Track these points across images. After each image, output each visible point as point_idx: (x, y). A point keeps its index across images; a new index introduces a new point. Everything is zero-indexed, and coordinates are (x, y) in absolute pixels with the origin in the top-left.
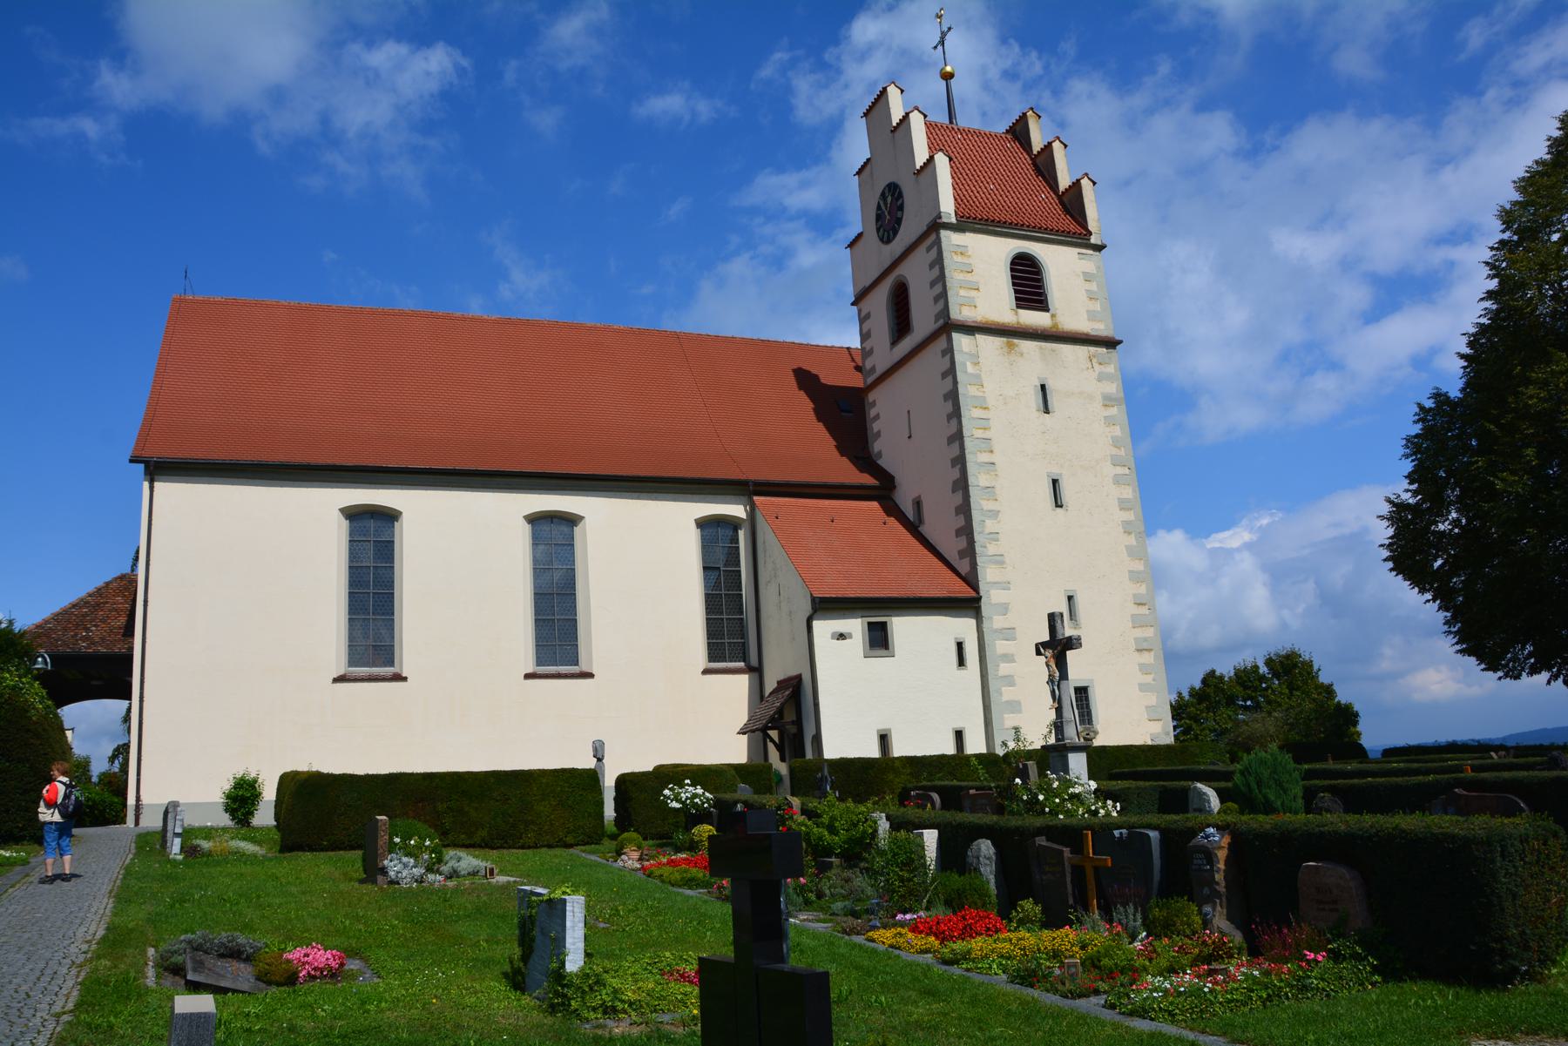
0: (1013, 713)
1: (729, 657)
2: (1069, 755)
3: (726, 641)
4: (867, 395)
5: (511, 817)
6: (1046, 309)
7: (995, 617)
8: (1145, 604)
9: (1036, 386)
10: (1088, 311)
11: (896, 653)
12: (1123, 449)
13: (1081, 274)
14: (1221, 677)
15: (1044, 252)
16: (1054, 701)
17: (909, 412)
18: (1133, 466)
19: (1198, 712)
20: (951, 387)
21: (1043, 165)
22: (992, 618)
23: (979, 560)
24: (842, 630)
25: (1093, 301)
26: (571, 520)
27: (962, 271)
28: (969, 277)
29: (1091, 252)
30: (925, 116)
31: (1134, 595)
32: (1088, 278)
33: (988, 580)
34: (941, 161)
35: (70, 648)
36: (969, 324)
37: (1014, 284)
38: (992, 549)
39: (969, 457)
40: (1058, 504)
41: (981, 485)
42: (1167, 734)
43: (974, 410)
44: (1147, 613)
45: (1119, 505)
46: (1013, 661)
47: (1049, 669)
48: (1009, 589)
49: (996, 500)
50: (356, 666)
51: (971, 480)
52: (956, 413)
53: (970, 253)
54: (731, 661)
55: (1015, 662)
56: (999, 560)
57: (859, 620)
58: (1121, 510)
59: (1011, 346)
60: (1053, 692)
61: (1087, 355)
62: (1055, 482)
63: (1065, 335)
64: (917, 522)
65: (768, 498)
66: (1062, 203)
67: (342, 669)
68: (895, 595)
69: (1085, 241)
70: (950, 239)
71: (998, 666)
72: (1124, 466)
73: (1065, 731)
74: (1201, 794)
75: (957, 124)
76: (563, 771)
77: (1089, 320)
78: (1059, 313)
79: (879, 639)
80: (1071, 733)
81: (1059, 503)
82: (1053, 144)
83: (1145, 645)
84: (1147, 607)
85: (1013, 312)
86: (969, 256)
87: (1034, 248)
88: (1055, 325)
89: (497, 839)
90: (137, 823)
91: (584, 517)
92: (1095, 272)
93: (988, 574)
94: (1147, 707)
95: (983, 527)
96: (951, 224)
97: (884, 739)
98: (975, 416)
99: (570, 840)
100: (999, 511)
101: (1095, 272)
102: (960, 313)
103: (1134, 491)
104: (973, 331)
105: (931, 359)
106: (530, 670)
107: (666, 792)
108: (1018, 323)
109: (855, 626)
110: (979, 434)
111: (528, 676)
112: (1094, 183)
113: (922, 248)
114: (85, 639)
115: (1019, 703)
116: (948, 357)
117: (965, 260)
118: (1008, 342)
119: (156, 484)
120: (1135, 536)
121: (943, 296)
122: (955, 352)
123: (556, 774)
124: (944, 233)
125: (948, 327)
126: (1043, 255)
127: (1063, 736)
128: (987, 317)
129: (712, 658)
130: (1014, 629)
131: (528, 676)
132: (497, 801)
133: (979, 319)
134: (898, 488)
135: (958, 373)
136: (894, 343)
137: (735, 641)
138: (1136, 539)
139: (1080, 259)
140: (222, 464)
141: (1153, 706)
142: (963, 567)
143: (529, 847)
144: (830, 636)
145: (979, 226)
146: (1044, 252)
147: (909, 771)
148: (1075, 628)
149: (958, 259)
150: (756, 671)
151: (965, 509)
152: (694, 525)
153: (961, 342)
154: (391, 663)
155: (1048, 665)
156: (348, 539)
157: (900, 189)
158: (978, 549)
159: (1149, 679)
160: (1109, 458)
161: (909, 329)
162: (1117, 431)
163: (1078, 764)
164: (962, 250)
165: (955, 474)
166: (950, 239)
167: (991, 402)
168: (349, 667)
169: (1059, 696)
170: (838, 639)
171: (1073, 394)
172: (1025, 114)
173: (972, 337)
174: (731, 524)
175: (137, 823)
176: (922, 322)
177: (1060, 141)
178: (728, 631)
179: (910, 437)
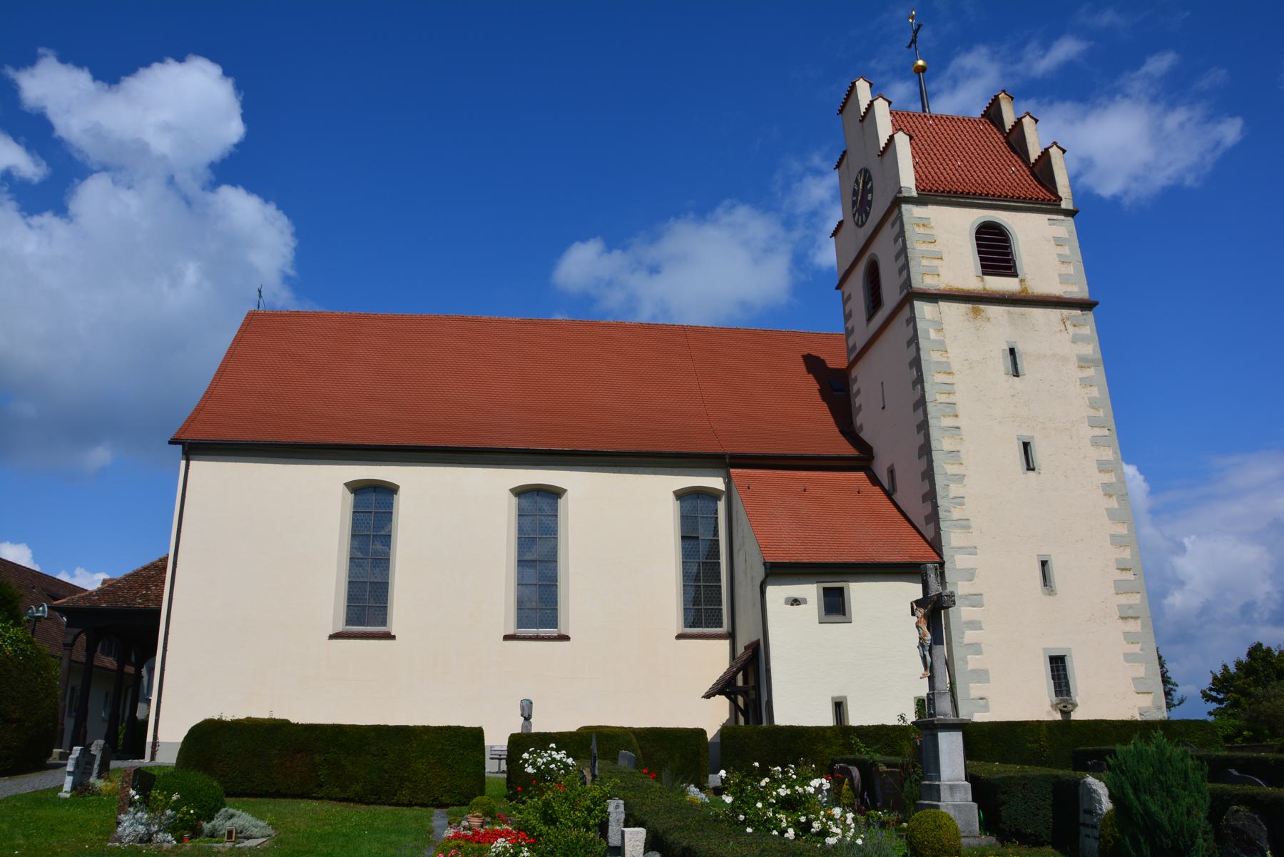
0: (979, 682)
1: (705, 623)
2: (939, 734)
3: (703, 607)
4: (850, 372)
5: (386, 773)
6: (1015, 275)
7: (959, 583)
8: (1130, 570)
9: (1004, 350)
10: (1060, 275)
11: (853, 618)
12: (1101, 410)
13: (1052, 239)
14: (1269, 650)
15: (1014, 222)
16: (926, 670)
17: (882, 383)
18: (1113, 427)
19: (1246, 686)
20: (914, 354)
21: (1016, 140)
22: (957, 583)
23: (942, 525)
24: (797, 595)
25: (1066, 265)
26: (554, 494)
27: (924, 242)
28: (931, 247)
29: (1062, 217)
30: (890, 103)
31: (1117, 560)
32: (1059, 242)
33: (952, 545)
34: (902, 141)
35: (127, 604)
36: (931, 292)
37: (979, 252)
38: (956, 514)
39: (931, 422)
40: (1030, 467)
41: (944, 449)
42: (1159, 708)
43: (938, 375)
44: (1133, 579)
45: (1098, 468)
46: (981, 628)
47: (919, 631)
48: (976, 554)
49: (962, 464)
50: (353, 625)
51: (934, 445)
52: (919, 380)
53: (932, 224)
54: (708, 627)
55: (982, 629)
56: (965, 525)
57: (815, 585)
58: (1100, 471)
59: (977, 312)
60: (924, 658)
61: (1059, 317)
62: (1026, 446)
63: (1035, 298)
64: (891, 490)
65: (745, 470)
66: (1033, 174)
67: (340, 627)
68: (852, 560)
69: (1055, 207)
70: (911, 213)
71: (964, 633)
72: (1103, 427)
73: (937, 705)
74: (1091, 792)
75: (930, 112)
76: (449, 728)
77: (1061, 283)
78: (1028, 277)
79: (835, 605)
80: (944, 705)
81: (1031, 466)
82: (1023, 120)
83: (1130, 613)
84: (1132, 572)
85: (979, 279)
86: (932, 227)
87: (1000, 217)
88: (1025, 290)
89: (371, 795)
90: (153, 758)
91: (566, 490)
92: (1067, 236)
93: (952, 539)
94: (1134, 679)
95: (947, 491)
96: (912, 197)
97: (839, 707)
98: (939, 381)
99: (445, 799)
100: (964, 475)
101: (1067, 236)
102: (923, 282)
103: (1115, 453)
104: (937, 299)
105: (898, 330)
106: (511, 631)
107: (526, 755)
108: (984, 289)
109: (811, 592)
110: (942, 398)
111: (507, 638)
112: (1064, 151)
113: (888, 226)
114: (143, 596)
115: (986, 672)
116: (911, 325)
117: (928, 231)
118: (973, 308)
119: (192, 463)
120: (1117, 498)
121: (906, 267)
122: (917, 320)
123: (439, 731)
124: (905, 207)
125: (912, 296)
126: (1010, 223)
127: (934, 710)
128: (950, 285)
129: (689, 624)
130: (981, 595)
131: (507, 638)
132: (375, 756)
133: (942, 286)
134: (875, 459)
135: (920, 340)
136: (869, 319)
137: (712, 607)
138: (1119, 503)
139: (1050, 225)
140: (245, 444)
141: (1143, 678)
142: (930, 534)
143: (403, 805)
144: (783, 601)
145: (941, 198)
146: (1014, 222)
147: (841, 741)
148: (1050, 595)
149: (921, 230)
150: (731, 636)
151: (929, 475)
152: (672, 497)
153: (924, 310)
154: (384, 623)
155: (918, 627)
156: (352, 510)
157: (869, 173)
158: (942, 514)
159: (1136, 648)
160: (1086, 419)
161: (880, 305)
162: (1095, 392)
163: (951, 748)
164: (925, 222)
165: (920, 440)
166: (911, 213)
167: (955, 367)
168: (347, 625)
169: (932, 663)
170: (792, 605)
171: (1045, 356)
172: (997, 97)
173: (936, 305)
174: (712, 495)
175: (153, 758)
176: (890, 296)
177: (1031, 117)
178: (705, 598)
179: (883, 408)
